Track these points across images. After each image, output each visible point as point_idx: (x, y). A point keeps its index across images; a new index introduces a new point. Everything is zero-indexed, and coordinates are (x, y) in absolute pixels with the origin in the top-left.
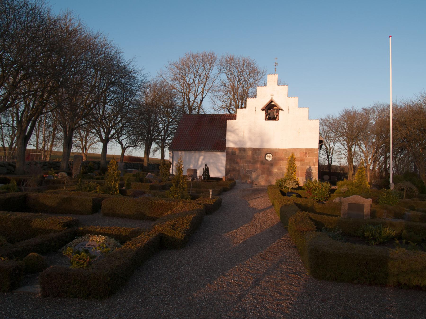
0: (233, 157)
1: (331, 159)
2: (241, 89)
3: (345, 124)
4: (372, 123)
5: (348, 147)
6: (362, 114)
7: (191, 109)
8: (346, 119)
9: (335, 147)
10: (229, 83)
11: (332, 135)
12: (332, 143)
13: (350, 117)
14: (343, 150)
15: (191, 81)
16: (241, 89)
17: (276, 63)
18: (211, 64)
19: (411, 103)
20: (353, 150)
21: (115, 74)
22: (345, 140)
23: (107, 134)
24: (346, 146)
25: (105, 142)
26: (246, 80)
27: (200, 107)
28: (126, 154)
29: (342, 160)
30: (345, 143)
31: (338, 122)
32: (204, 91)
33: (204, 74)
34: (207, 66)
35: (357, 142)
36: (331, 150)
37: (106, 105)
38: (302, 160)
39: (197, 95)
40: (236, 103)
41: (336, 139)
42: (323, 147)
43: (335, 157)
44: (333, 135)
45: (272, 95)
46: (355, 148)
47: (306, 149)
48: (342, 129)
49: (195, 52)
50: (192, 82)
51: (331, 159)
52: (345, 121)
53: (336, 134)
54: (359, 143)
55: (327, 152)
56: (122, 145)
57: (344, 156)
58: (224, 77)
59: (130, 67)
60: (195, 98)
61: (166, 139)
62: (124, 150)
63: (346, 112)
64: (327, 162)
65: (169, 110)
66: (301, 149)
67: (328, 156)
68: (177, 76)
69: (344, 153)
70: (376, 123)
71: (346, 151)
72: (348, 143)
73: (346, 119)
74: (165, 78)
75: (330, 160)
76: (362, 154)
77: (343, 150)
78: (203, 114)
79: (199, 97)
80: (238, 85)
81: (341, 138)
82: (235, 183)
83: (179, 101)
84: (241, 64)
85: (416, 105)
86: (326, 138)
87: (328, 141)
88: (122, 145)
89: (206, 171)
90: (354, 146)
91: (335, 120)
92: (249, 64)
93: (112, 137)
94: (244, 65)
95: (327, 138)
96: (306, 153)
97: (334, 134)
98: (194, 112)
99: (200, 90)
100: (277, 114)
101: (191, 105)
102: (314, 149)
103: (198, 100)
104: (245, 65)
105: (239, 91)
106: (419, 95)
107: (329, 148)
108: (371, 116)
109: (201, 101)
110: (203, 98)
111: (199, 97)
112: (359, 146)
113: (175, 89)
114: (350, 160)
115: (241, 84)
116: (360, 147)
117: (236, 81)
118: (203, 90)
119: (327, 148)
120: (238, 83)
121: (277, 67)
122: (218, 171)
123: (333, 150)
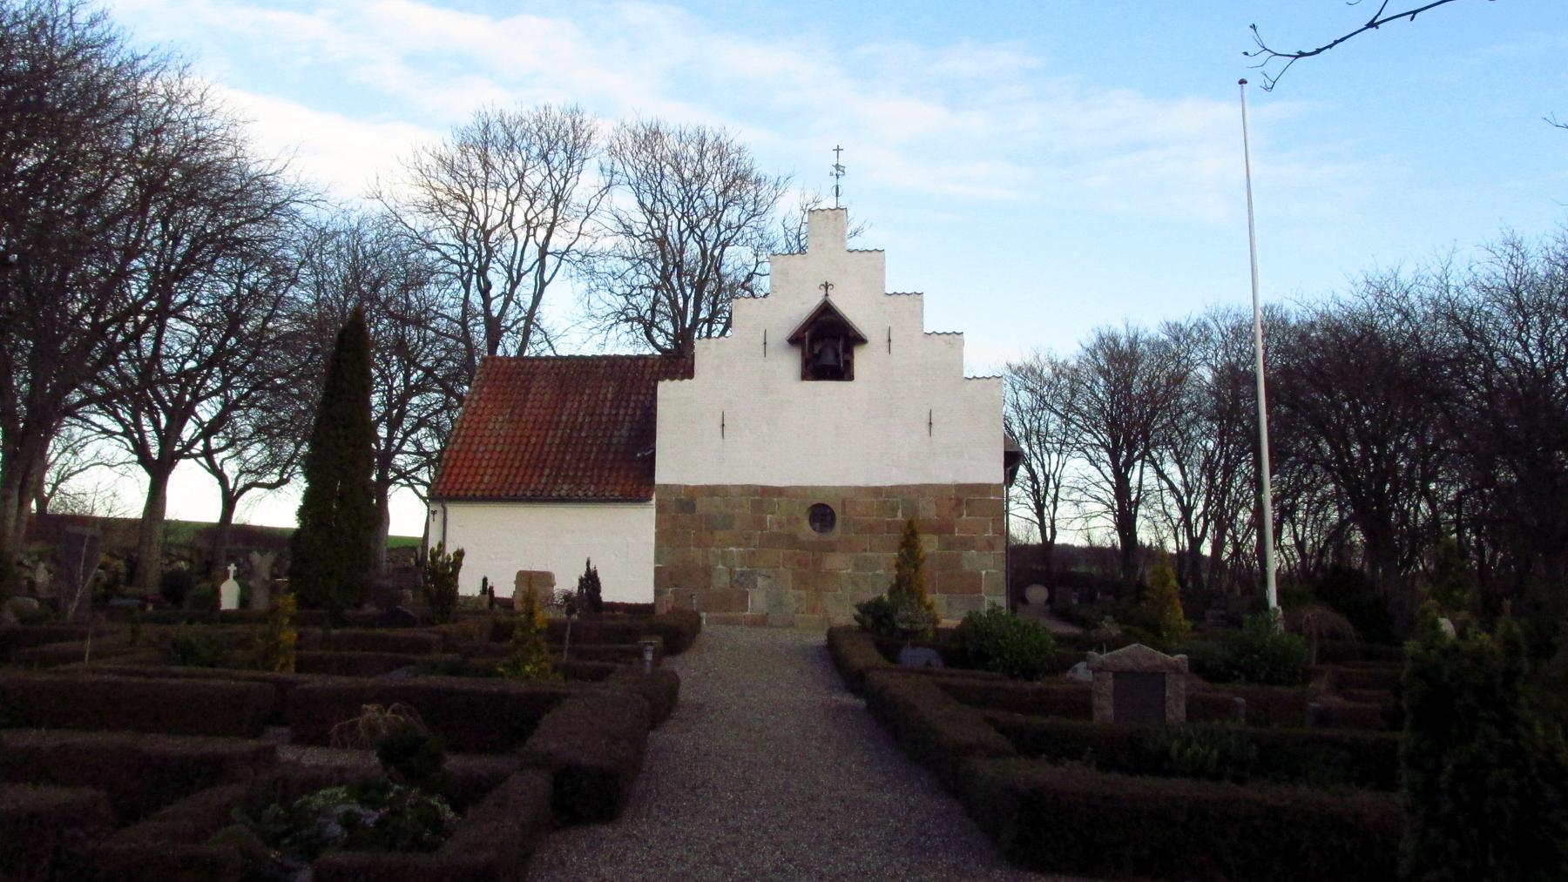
0: (687, 516)
1: (1053, 521)
2: (693, 249)
3: (1101, 381)
4: (1202, 378)
5: (1117, 472)
6: (1165, 345)
7: (495, 330)
8: (1102, 362)
9: (1065, 473)
10: (643, 228)
11: (1052, 427)
12: (1054, 456)
13: (1119, 359)
14: (1097, 484)
15: (496, 217)
16: (693, 249)
17: (837, 167)
18: (575, 151)
19: (1333, 307)
20: (1134, 482)
21: (204, 199)
22: (1103, 445)
23: (168, 437)
24: (1108, 471)
25: (159, 471)
26: (715, 215)
27: (530, 317)
28: (238, 517)
29: (1093, 522)
30: (1106, 456)
31: (1075, 376)
32: (549, 259)
33: (547, 188)
34: (558, 158)
35: (1146, 451)
36: (1051, 484)
37: (171, 321)
38: (943, 529)
39: (520, 276)
40: (674, 303)
41: (1069, 440)
42: (1022, 471)
43: (1065, 510)
44: (1054, 423)
45: (826, 286)
46: (1142, 476)
47: (961, 488)
48: (1089, 403)
49: (511, 111)
50: (498, 221)
51: (1053, 521)
52: (1101, 371)
53: (1069, 421)
54: (1154, 454)
55: (1036, 492)
56: (223, 480)
57: (1101, 507)
58: (625, 201)
59: (287, 181)
60: (515, 285)
61: (399, 450)
62: (229, 500)
63: (1102, 339)
64: (1037, 529)
65: (412, 332)
66: (941, 488)
67: (1040, 508)
68: (440, 195)
69: (1102, 495)
70: (1215, 378)
71: (1108, 486)
72: (1114, 455)
73: (1102, 362)
74: (391, 204)
75: (1048, 522)
76: (1170, 500)
77: (1097, 484)
78: (548, 358)
79: (528, 282)
80: (681, 233)
81: (1088, 437)
82: (695, 628)
83: (446, 297)
84: (692, 151)
85: (1353, 317)
86: (1028, 438)
87: (1036, 449)
88: (223, 480)
89: (591, 581)
90: (1138, 463)
91: (1058, 372)
92: (721, 153)
93: (187, 452)
94: (702, 154)
95: (1034, 439)
96: (959, 501)
97: (1058, 421)
98: (508, 346)
99: (532, 253)
100: (847, 357)
101: (495, 314)
102: (989, 486)
103: (525, 292)
104: (709, 155)
105: (687, 256)
106: (1360, 279)
107: (1041, 478)
108: (1196, 355)
109: (537, 298)
110: (543, 284)
111: (528, 282)
112: (1156, 467)
113: (431, 246)
114: (1126, 523)
115: (692, 228)
116: (1161, 475)
117: (672, 218)
118: (543, 252)
119: (1034, 478)
120: (683, 226)
121: (841, 181)
122: (630, 580)
123: (1057, 487)
